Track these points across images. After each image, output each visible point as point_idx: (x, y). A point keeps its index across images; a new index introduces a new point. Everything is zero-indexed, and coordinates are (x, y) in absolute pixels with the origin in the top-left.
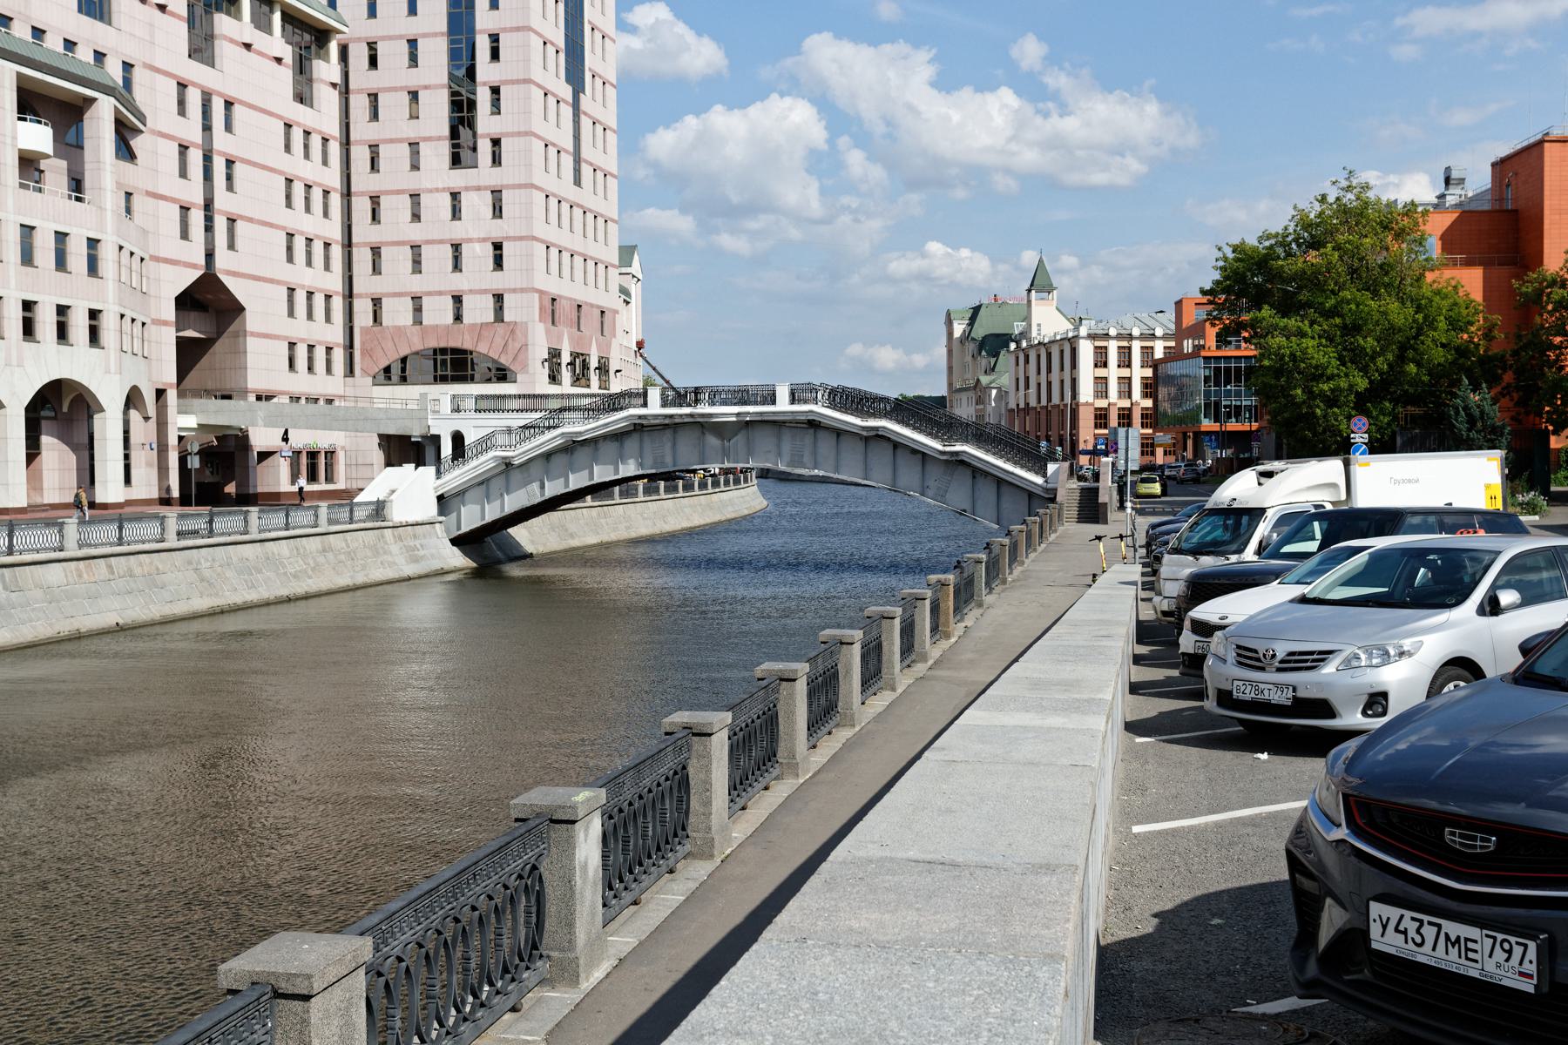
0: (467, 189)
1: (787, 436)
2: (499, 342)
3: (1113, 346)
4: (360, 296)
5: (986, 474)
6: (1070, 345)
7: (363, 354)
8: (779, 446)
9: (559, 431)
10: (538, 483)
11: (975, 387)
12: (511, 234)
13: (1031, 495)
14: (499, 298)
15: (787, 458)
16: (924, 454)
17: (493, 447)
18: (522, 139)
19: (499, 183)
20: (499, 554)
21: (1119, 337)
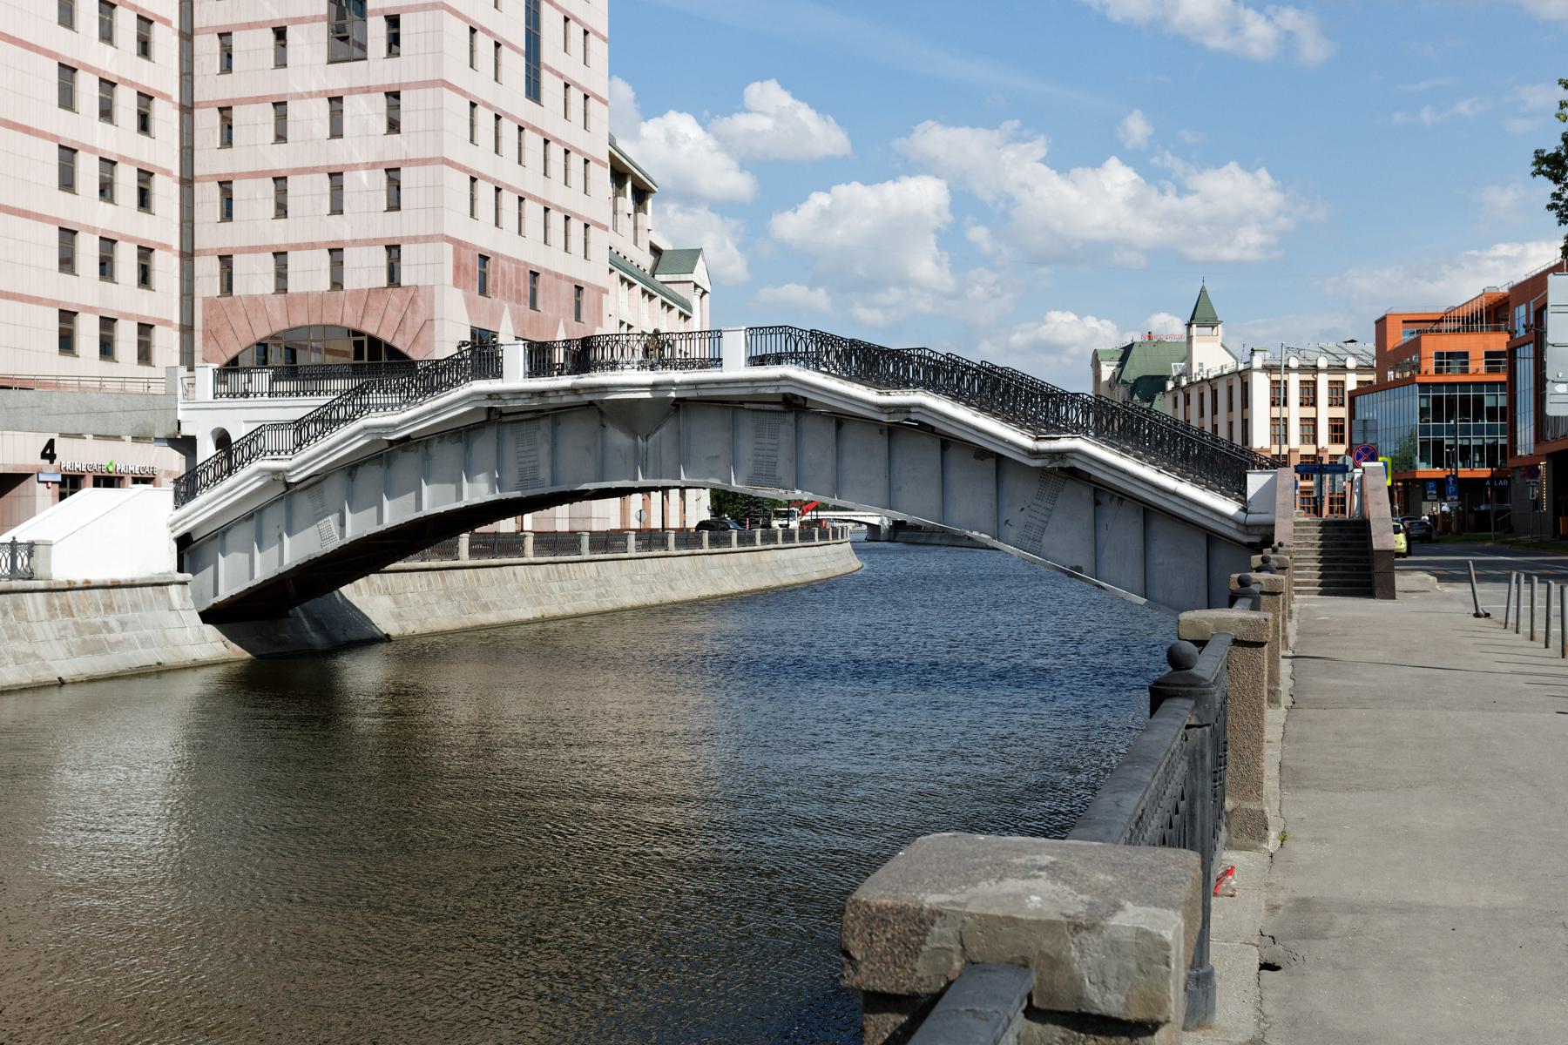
0: (351, 91)
1: (747, 425)
2: (393, 315)
3: (1294, 381)
4: (203, 253)
5: (1122, 497)
6: (1241, 380)
7: (205, 338)
8: (733, 445)
10: (337, 515)
13: (1212, 538)
14: (393, 250)
15: (747, 468)
16: (999, 457)
17: (261, 452)
18: (430, 14)
19: (397, 81)
20: (316, 639)
21: (1301, 369)
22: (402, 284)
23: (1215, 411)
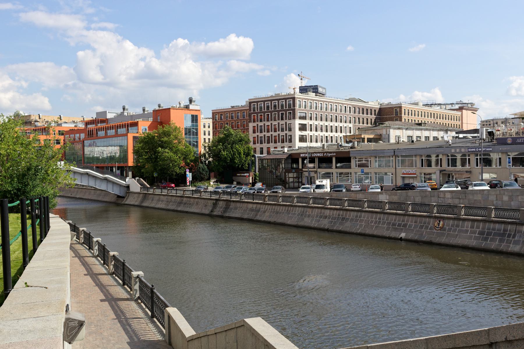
16: (96, 177)
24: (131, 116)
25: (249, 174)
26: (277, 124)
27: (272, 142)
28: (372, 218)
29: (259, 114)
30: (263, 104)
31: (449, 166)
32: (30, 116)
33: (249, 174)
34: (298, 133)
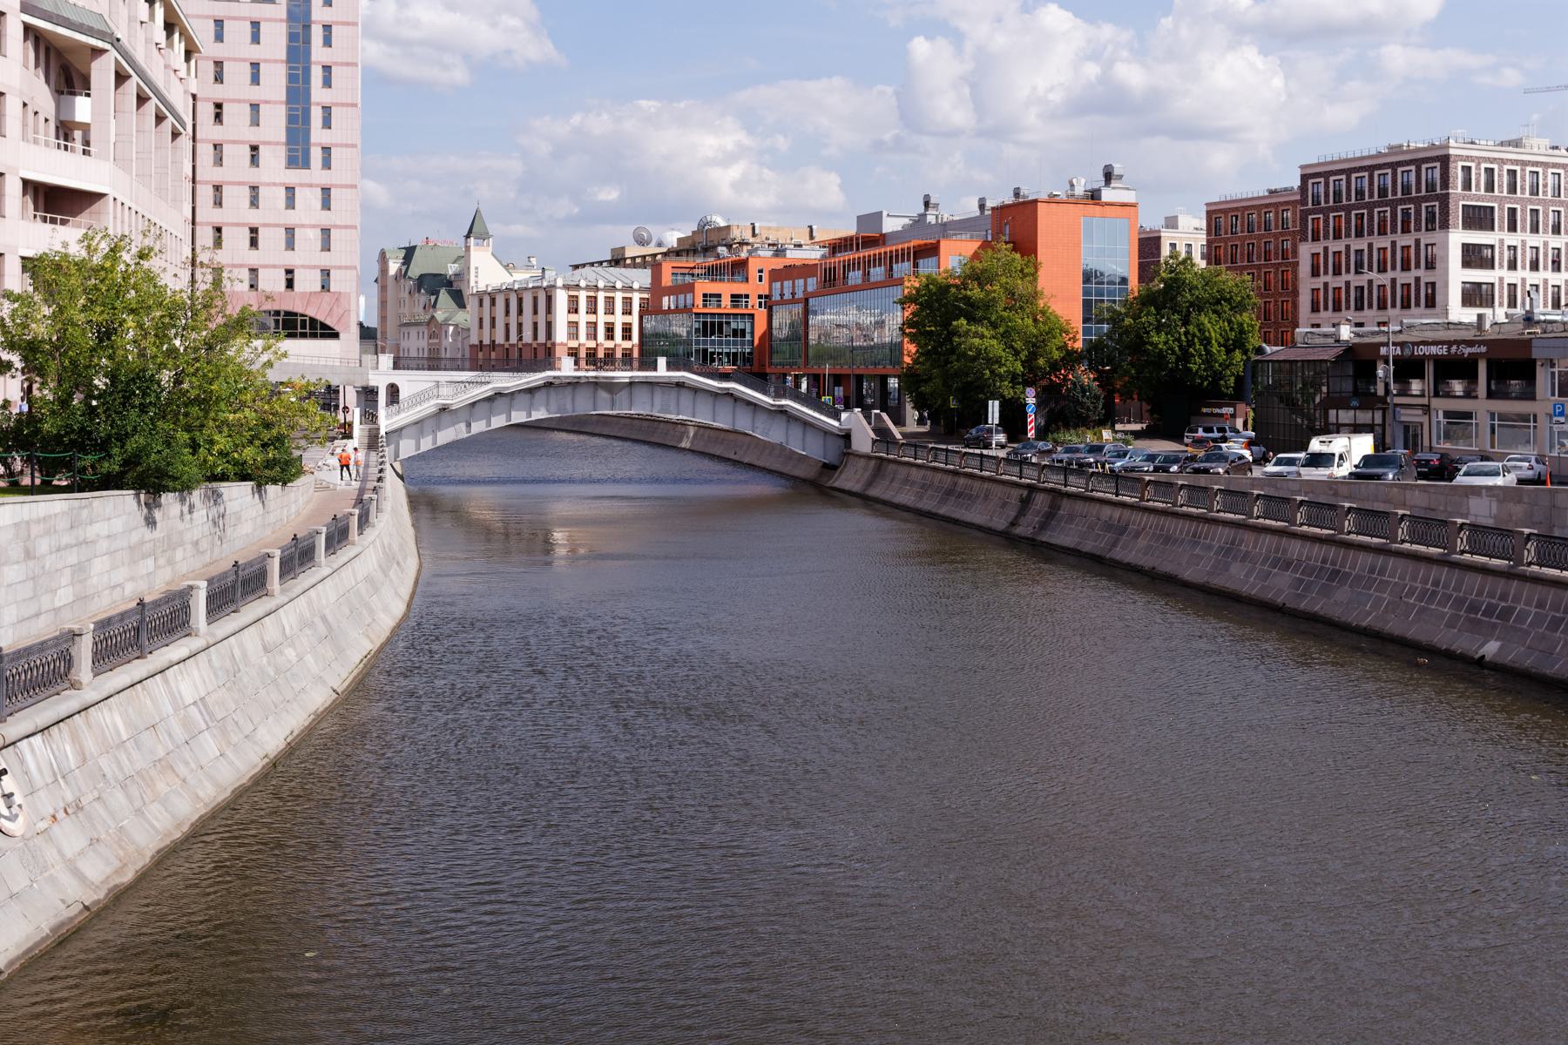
2: (325, 307)
9: (490, 386)
11: (428, 323)
12: (338, 223)
16: (756, 405)
21: (588, 288)
22: (331, 290)
23: (520, 312)
24: (941, 225)
25: (1235, 410)
26: (1343, 249)
27: (1370, 306)
28: (1414, 579)
29: (1331, 215)
30: (1390, 176)
31: (1553, 394)
32: (728, 228)
33: (1235, 410)
34: (1457, 276)
